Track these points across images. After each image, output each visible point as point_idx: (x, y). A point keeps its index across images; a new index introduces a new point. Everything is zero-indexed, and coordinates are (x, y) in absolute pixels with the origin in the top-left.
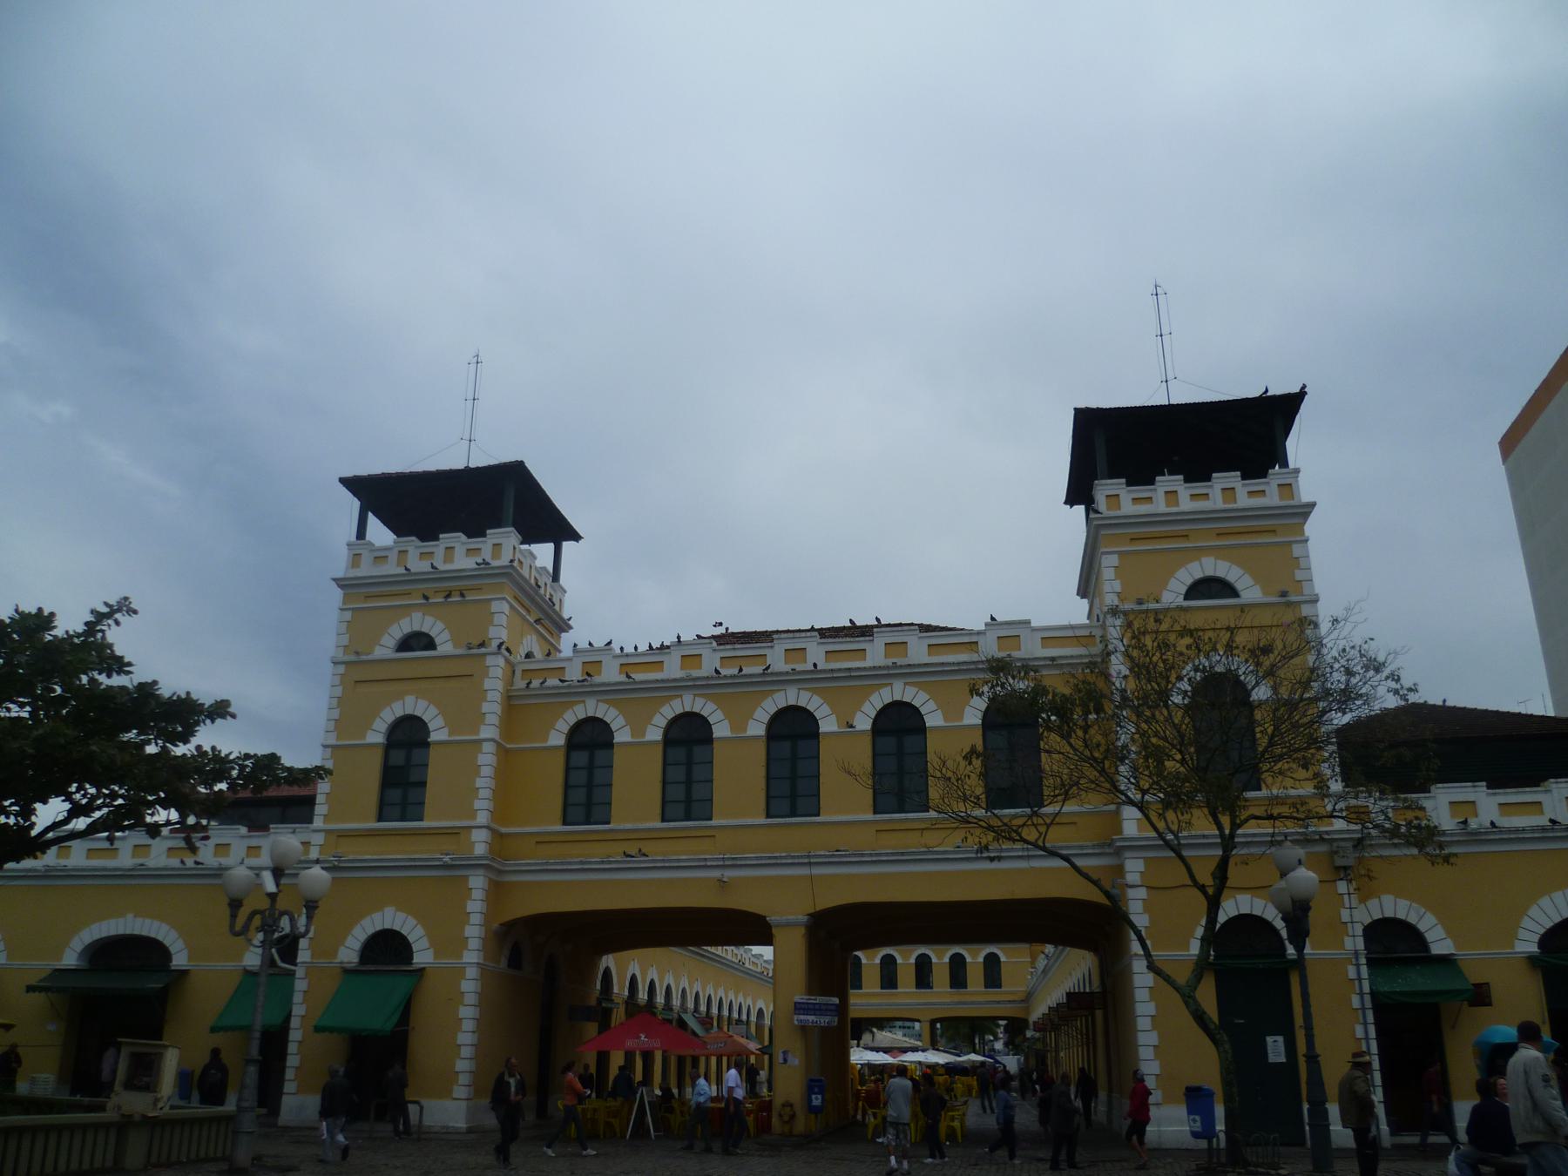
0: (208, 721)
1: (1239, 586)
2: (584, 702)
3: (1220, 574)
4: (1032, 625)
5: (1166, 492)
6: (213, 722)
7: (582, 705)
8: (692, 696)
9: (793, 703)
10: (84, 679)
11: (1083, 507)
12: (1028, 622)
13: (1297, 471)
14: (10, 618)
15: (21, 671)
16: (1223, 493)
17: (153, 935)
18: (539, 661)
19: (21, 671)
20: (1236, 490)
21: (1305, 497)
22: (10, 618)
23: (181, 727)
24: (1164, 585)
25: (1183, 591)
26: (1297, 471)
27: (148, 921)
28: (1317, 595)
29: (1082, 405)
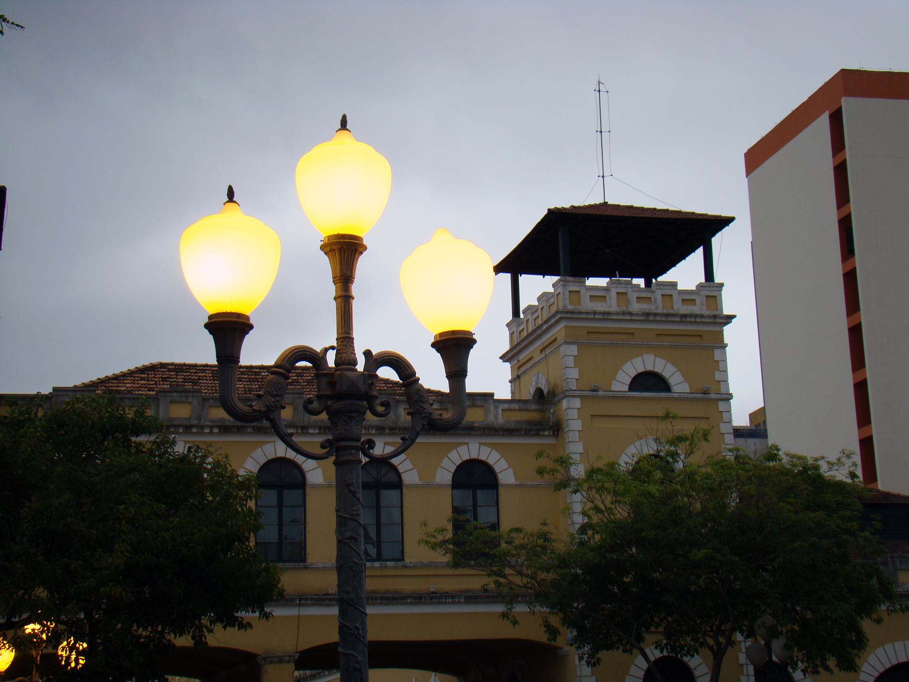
0: (237, 627)
1: (672, 381)
2: (467, 444)
3: (658, 369)
4: (495, 398)
5: (618, 293)
6: (239, 629)
7: (466, 446)
8: (478, 444)
9: (476, 457)
10: (225, 620)
11: (510, 274)
12: (492, 395)
13: (721, 285)
14: (564, 627)
15: (40, 611)
16: (706, 298)
17: (894, 662)
18: (683, 399)
19: (40, 611)
20: (673, 296)
21: (726, 311)
22: (564, 627)
23: (652, 281)
24: (613, 377)
25: (628, 382)
26: (721, 285)
27: (889, 647)
28: (731, 395)
29: (552, 207)
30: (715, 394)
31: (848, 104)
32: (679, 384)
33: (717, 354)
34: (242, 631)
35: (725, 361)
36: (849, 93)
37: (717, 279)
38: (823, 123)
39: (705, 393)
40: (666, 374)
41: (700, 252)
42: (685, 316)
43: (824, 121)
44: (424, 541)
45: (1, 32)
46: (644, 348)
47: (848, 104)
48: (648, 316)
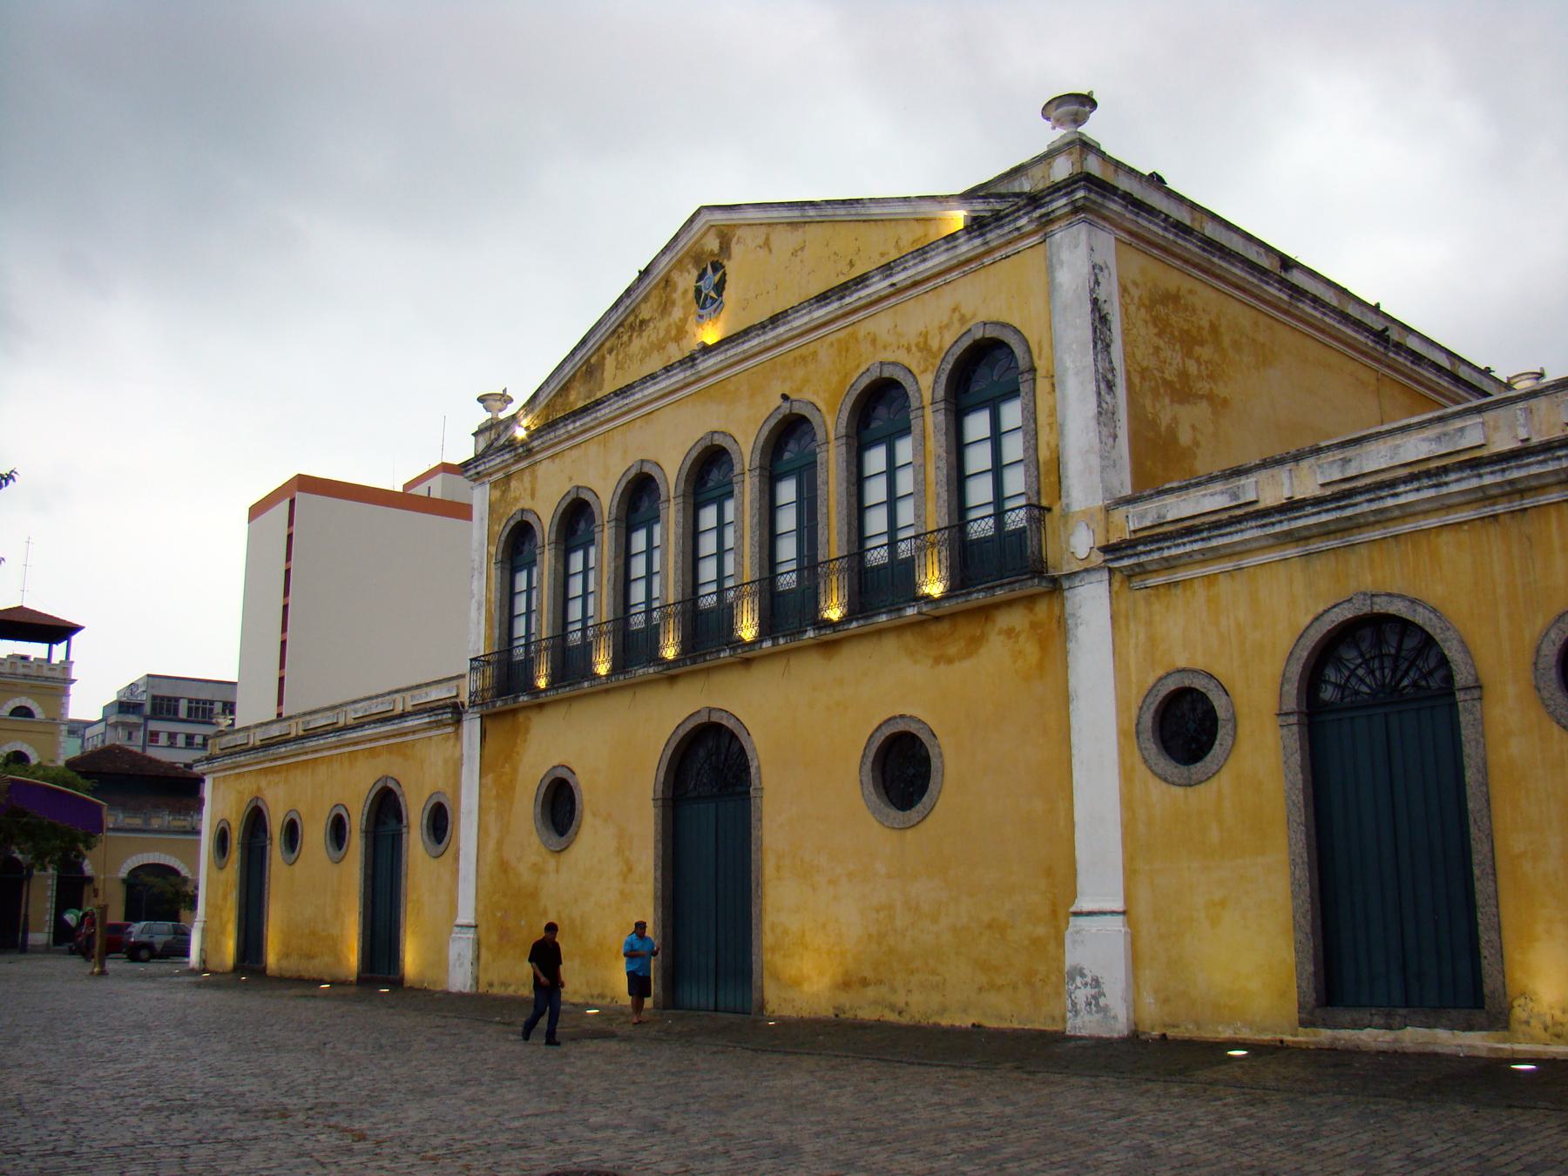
1: (35, 712)
18: (41, 722)
21: (73, 678)
30: (970, 330)
31: (299, 496)
32: (39, 714)
33: (64, 700)
34: (942, 667)
35: (68, 703)
36: (300, 490)
37: (71, 659)
38: (284, 505)
39: (54, 720)
40: (32, 708)
41: (66, 642)
42: (47, 678)
43: (285, 504)
44: (914, 349)
45: (1564, 1012)
46: (22, 693)
47: (299, 496)
48: (26, 676)
